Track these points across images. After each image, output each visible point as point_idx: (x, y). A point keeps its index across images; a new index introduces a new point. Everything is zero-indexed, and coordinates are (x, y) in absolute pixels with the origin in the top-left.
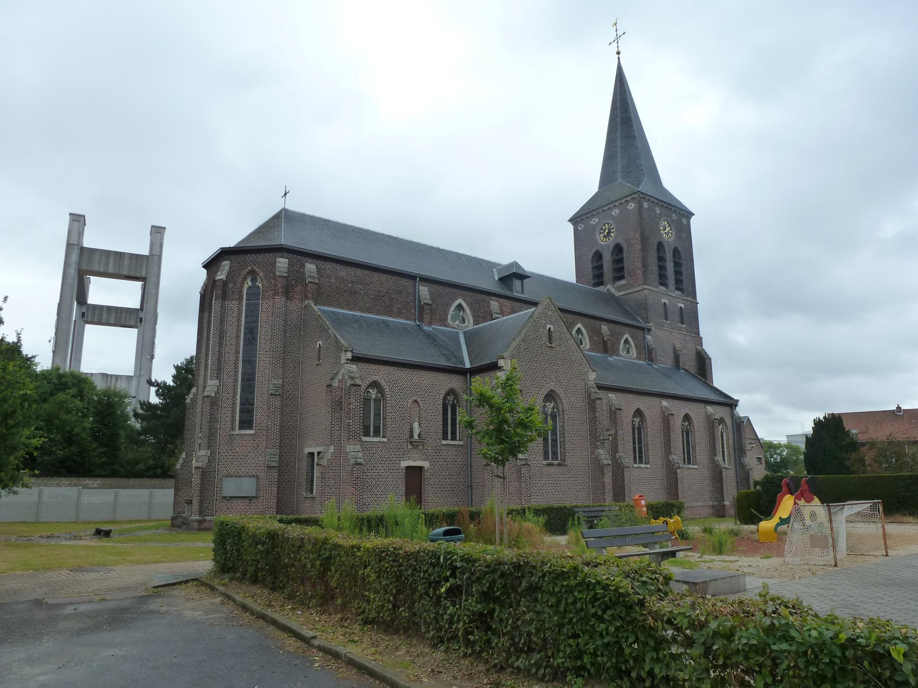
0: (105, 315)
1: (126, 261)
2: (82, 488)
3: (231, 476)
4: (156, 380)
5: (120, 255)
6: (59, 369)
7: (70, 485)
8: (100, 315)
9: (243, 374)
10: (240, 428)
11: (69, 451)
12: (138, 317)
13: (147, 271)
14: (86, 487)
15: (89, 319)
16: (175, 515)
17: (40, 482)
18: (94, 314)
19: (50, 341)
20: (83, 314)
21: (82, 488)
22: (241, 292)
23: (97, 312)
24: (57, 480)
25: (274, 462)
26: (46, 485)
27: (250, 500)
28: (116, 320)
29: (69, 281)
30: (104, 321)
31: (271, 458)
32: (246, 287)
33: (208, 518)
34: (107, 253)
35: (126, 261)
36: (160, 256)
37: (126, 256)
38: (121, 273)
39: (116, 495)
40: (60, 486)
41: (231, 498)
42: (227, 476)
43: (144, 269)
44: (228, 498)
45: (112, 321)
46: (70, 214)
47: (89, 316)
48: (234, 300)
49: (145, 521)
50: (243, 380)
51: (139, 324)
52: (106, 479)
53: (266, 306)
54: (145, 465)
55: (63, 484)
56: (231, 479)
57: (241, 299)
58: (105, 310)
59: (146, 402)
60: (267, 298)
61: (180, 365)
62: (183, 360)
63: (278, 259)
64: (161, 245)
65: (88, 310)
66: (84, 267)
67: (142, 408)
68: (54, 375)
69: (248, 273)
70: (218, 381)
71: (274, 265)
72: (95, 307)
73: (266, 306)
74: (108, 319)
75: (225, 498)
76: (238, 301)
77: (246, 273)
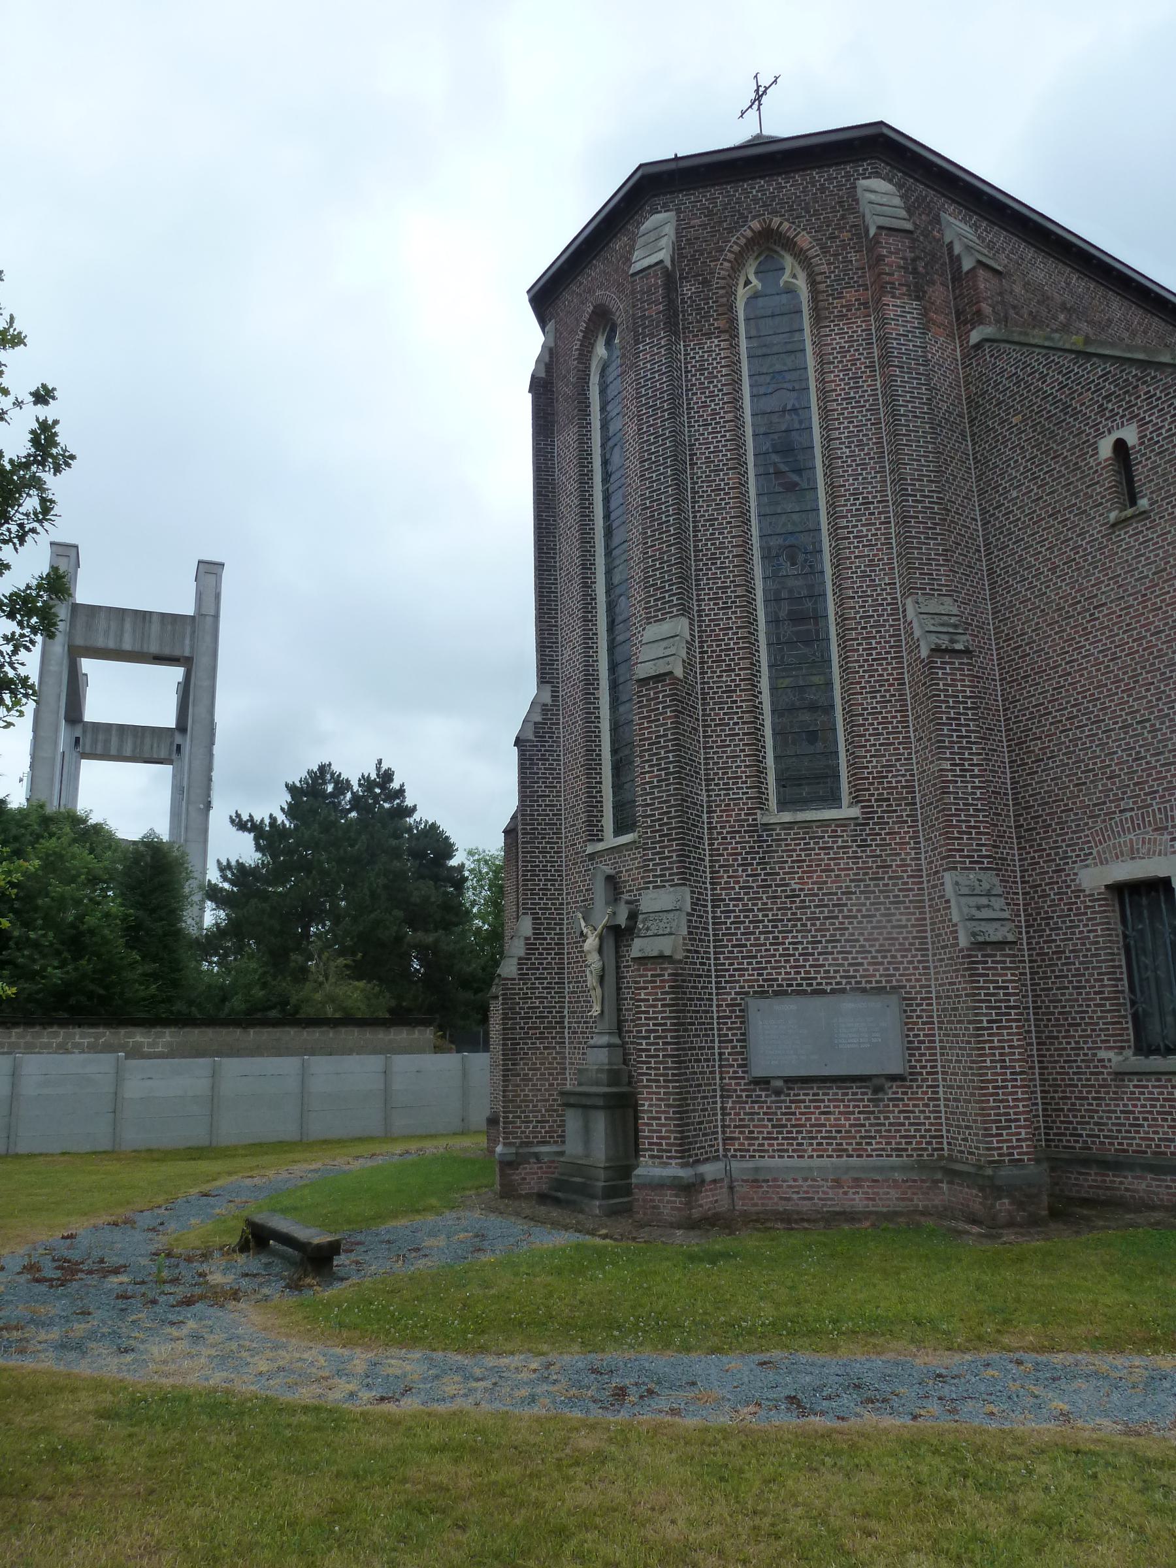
0: (114, 740)
1: (155, 627)
2: (126, 1058)
3: (777, 994)
4: (250, 816)
5: (143, 617)
6: (42, 806)
7: (93, 1048)
8: (107, 742)
9: (773, 599)
10: (783, 805)
11: (76, 969)
12: (172, 743)
13: (192, 647)
14: (135, 1053)
15: (88, 750)
16: (513, 1150)
17: (13, 1039)
18: (95, 742)
19: (21, 780)
20: (77, 740)
21: (126, 1058)
22: (731, 307)
23: (101, 737)
24: (59, 1035)
25: (996, 925)
26: (30, 1049)
27: (875, 1092)
28: (134, 751)
29: (53, 668)
30: (113, 752)
31: (979, 908)
32: (742, 294)
33: (709, 1170)
34: (120, 614)
35: (155, 627)
36: (216, 617)
37: (155, 619)
38: (145, 650)
39: (214, 1074)
40: (67, 1052)
41: (790, 1081)
42: (762, 994)
43: (187, 642)
44: (779, 1083)
45: (128, 751)
46: (52, 544)
47: (87, 746)
48: (709, 335)
49: (280, 1147)
50: (774, 621)
51: (174, 756)
52: (186, 1030)
53: (838, 341)
54: (246, 1001)
55: (76, 1045)
56: (789, 1006)
57: (731, 331)
58: (114, 732)
59: (233, 863)
60: (842, 316)
61: (298, 784)
62: (304, 774)
63: (863, 183)
64: (218, 597)
65: (84, 732)
66: (79, 641)
67: (225, 878)
68: (33, 817)
69: (751, 243)
70: (685, 621)
71: (850, 202)
72: (96, 726)
73: (838, 341)
74: (120, 748)
75: (763, 1082)
76: (725, 336)
77: (743, 241)
